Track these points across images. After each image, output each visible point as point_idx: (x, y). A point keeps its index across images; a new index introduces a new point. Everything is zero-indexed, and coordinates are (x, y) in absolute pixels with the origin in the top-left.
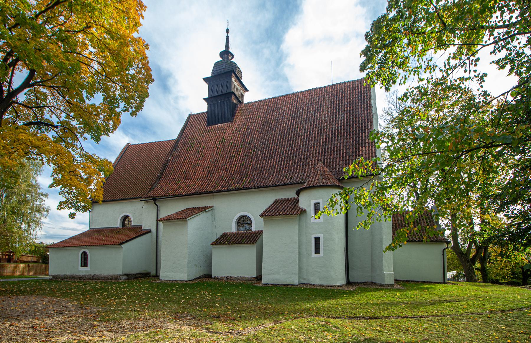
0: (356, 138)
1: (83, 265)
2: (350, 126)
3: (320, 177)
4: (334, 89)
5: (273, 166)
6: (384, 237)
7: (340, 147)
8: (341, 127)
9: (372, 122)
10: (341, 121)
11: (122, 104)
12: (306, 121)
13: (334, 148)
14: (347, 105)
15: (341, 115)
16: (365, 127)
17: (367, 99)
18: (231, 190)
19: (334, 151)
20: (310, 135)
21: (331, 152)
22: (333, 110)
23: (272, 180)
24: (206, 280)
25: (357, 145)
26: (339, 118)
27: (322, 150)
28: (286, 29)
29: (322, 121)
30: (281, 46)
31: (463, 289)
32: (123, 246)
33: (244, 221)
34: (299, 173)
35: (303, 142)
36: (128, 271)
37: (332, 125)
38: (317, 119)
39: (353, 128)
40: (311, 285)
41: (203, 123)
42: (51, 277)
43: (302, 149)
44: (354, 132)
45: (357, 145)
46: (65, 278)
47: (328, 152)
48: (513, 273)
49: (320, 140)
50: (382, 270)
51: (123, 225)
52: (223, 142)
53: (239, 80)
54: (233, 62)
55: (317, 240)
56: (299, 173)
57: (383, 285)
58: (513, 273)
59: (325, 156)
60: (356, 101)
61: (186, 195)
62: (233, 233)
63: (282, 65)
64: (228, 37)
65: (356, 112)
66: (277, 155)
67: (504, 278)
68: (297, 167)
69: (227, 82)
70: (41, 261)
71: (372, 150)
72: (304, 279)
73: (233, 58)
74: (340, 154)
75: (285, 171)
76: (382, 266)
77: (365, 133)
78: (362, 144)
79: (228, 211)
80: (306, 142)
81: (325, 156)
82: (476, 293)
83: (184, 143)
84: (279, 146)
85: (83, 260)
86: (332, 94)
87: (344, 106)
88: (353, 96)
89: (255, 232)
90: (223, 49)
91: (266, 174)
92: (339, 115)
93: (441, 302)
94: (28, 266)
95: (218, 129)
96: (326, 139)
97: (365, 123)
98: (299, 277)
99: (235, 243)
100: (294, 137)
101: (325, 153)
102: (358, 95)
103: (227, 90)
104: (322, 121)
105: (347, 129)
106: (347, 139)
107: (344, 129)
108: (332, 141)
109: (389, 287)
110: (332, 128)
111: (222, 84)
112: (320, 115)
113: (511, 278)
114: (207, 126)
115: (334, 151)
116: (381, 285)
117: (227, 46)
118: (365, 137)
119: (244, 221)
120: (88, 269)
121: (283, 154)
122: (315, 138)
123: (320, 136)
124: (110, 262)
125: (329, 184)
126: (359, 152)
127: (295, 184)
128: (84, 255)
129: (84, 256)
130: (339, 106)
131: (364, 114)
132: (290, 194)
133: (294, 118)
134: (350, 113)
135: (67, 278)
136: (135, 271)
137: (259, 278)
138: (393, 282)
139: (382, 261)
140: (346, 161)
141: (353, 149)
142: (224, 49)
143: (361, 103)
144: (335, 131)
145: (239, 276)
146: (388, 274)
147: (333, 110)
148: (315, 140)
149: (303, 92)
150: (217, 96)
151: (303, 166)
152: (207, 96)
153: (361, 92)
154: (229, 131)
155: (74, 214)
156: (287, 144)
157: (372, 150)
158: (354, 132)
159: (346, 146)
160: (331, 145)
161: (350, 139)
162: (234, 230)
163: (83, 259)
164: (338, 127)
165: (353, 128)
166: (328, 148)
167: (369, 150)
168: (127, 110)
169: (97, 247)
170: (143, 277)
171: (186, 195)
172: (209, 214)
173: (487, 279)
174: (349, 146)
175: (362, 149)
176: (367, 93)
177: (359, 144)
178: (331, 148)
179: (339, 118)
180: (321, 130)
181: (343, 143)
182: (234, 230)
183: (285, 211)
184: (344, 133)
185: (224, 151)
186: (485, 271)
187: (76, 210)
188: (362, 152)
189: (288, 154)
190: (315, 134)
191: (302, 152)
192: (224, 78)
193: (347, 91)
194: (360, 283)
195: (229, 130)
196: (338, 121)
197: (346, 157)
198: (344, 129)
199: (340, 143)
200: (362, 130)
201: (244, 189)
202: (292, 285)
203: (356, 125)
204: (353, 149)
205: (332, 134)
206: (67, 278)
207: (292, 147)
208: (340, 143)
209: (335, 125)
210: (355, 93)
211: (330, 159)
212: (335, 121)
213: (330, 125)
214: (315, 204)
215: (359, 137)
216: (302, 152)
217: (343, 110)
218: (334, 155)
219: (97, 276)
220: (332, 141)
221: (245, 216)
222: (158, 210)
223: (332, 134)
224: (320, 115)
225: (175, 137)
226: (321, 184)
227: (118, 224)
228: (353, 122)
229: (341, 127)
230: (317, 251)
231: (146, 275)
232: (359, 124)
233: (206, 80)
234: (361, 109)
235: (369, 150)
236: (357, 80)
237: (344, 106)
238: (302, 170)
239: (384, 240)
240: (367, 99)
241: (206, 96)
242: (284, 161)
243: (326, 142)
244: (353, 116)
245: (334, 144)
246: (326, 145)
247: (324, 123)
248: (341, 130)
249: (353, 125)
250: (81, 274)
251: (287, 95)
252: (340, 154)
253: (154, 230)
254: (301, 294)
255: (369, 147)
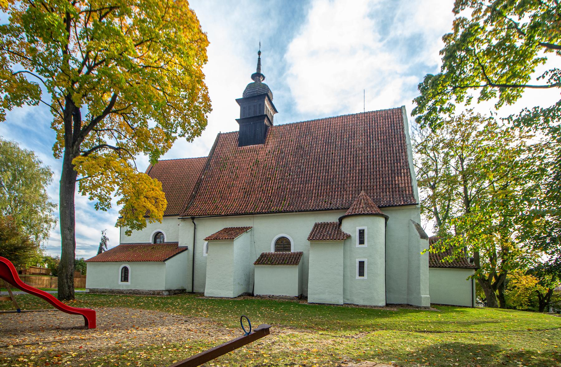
0: (391, 167)
1: (123, 280)
2: (385, 155)
3: (364, 206)
4: (367, 117)
5: (310, 190)
6: (421, 263)
7: (376, 175)
8: (376, 155)
9: (406, 152)
10: (376, 149)
11: (179, 130)
12: (341, 147)
13: (370, 176)
14: (381, 134)
15: (376, 143)
16: (400, 157)
17: (400, 129)
18: (271, 213)
19: (370, 179)
20: (345, 162)
21: (367, 180)
22: (367, 138)
23: (312, 204)
24: (249, 297)
25: (393, 175)
26: (373, 146)
27: (359, 177)
28: (290, 38)
29: (356, 149)
30: (285, 56)
31: (483, 313)
32: (166, 262)
33: (283, 244)
34: (337, 199)
35: (339, 168)
36: (169, 288)
37: (367, 153)
38: (351, 146)
39: (388, 158)
40: (354, 305)
41: (234, 144)
42: (88, 291)
43: (339, 175)
44: (389, 162)
45: (393, 175)
46: (103, 292)
47: (364, 180)
48: (530, 300)
49: (356, 167)
50: (419, 293)
51: (155, 242)
52: (257, 163)
53: (270, 101)
54: (265, 85)
55: (362, 264)
56: (337, 199)
57: (420, 307)
58: (530, 300)
59: (361, 183)
60: (389, 130)
61: (225, 215)
62: (272, 253)
63: (284, 75)
64: (259, 59)
65: (389, 142)
66: (314, 180)
67: (521, 305)
68: (335, 192)
69: (260, 105)
70: (51, 274)
71: (408, 180)
72: (348, 300)
73: (263, 79)
74: (377, 182)
75: (323, 196)
76: (420, 289)
77: (400, 163)
78: (398, 174)
79: (266, 232)
80: (342, 168)
81: (361, 183)
82: (507, 316)
83: (216, 163)
84: (315, 171)
85: (123, 275)
86: (365, 122)
87: (378, 134)
88: (386, 125)
89: (294, 253)
90: (255, 71)
91: (304, 197)
92: (373, 143)
93: (484, 322)
94: (51, 279)
95: (251, 150)
96: (362, 166)
97: (399, 153)
98: (344, 298)
99: (278, 264)
100: (329, 163)
101: (362, 180)
102: (391, 124)
103: (260, 111)
104: (356, 149)
105: (382, 158)
106: (382, 168)
107: (379, 158)
108: (368, 169)
109: (426, 309)
110: (367, 156)
111: (254, 106)
112: (354, 143)
113: (528, 305)
114: (239, 146)
115: (370, 179)
116: (418, 307)
117: (259, 68)
118: (400, 167)
119: (283, 244)
120: (128, 283)
121: (319, 180)
122: (350, 165)
123: (356, 163)
124: (152, 277)
125: (374, 212)
126: (395, 181)
127: (335, 209)
128: (125, 270)
129: (125, 271)
130: (373, 135)
131: (398, 144)
132: (332, 218)
133: (328, 143)
134: (384, 142)
135: (105, 292)
136: (174, 287)
137: (303, 296)
138: (429, 305)
139: (419, 285)
140: (383, 189)
141: (389, 178)
142: (255, 71)
143: (394, 132)
144: (370, 159)
145: (281, 294)
146: (425, 297)
147: (367, 138)
148: (350, 167)
149: (335, 118)
150: (250, 118)
151: (341, 192)
152: (239, 118)
153: (394, 122)
154: (262, 153)
155: (130, 232)
156: (323, 170)
157: (408, 180)
158: (389, 162)
159: (382, 175)
160: (367, 173)
161: (385, 168)
162: (272, 251)
163: (123, 273)
164: (373, 156)
165: (388, 158)
166: (364, 176)
167: (404, 180)
168: (184, 135)
169: (148, 262)
170: (181, 293)
171: (225, 215)
172: (249, 234)
173: (504, 305)
174: (385, 175)
175: (398, 178)
176: (399, 124)
177: (395, 174)
178: (367, 176)
179: (373, 146)
180: (356, 157)
181: (379, 172)
182: (272, 251)
183: (325, 235)
184: (379, 162)
185: (259, 173)
186: (503, 298)
187: (131, 227)
188: (398, 181)
189: (325, 179)
190: (350, 161)
191: (339, 178)
192: (256, 100)
193: (380, 120)
194: (396, 304)
195: (263, 152)
196: (373, 149)
197: (383, 185)
198: (379, 158)
199: (376, 172)
200: (397, 160)
201: (285, 212)
202: (337, 305)
203: (390, 154)
204: (389, 178)
205: (367, 162)
206: (105, 292)
207: (328, 173)
208: (376, 172)
209: (370, 153)
210: (388, 122)
211: (367, 187)
212: (370, 150)
213: (365, 153)
214: (360, 230)
215: (394, 167)
216: (339, 178)
217: (377, 138)
218: (370, 183)
219: (139, 291)
220: (368, 169)
221: (283, 237)
222: (195, 228)
223: (367, 162)
224: (354, 143)
225: (207, 154)
226: (366, 212)
227: (151, 241)
228: (387, 151)
229: (376, 155)
230: (361, 273)
231: (182, 291)
232: (393, 154)
233: (238, 101)
234: (395, 138)
235: (404, 180)
236: (389, 110)
237: (378, 134)
238: (340, 196)
239: (421, 265)
240: (400, 129)
241: (238, 117)
242: (322, 186)
243: (362, 170)
244: (387, 145)
245: (370, 172)
246: (362, 173)
247: (359, 151)
248: (376, 158)
249: (388, 154)
250: (121, 288)
251: (319, 120)
252: (377, 182)
253: (191, 248)
254: (345, 314)
255: (404, 177)
